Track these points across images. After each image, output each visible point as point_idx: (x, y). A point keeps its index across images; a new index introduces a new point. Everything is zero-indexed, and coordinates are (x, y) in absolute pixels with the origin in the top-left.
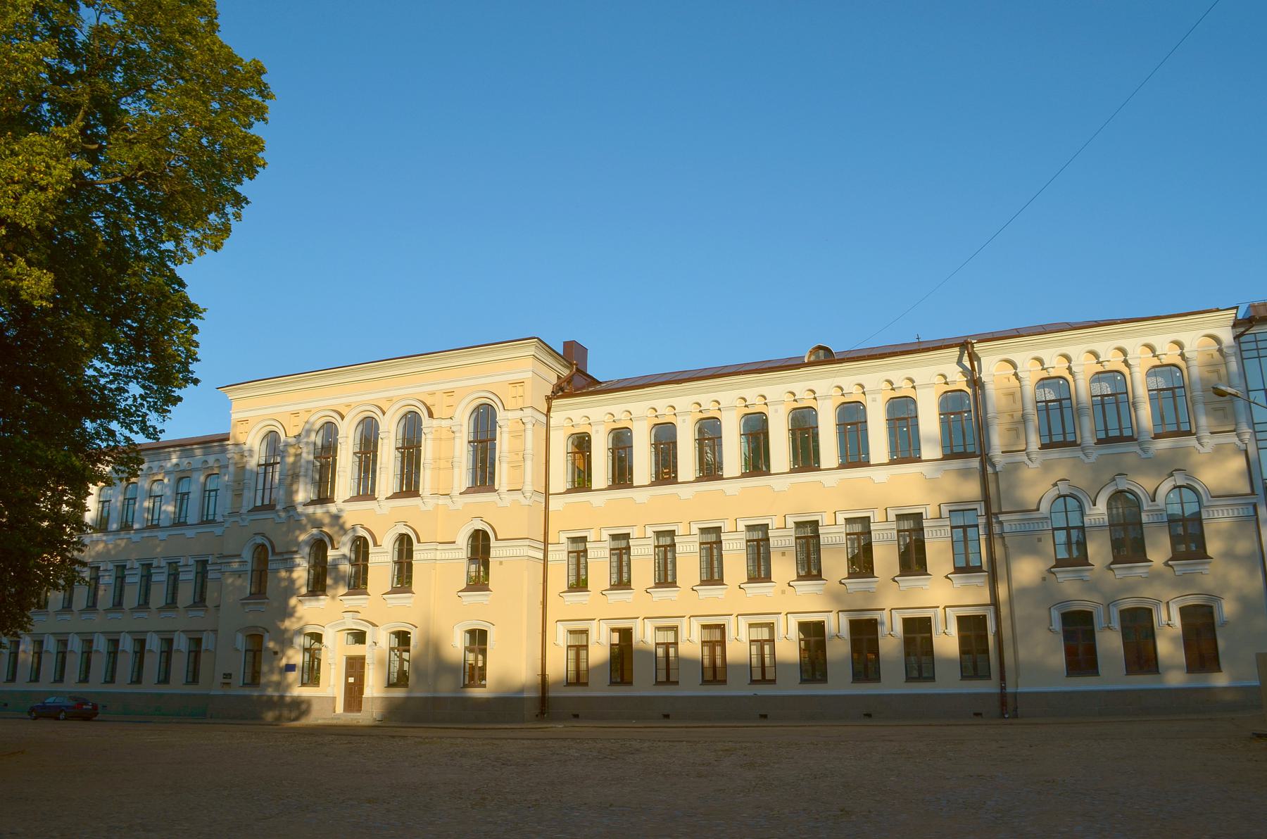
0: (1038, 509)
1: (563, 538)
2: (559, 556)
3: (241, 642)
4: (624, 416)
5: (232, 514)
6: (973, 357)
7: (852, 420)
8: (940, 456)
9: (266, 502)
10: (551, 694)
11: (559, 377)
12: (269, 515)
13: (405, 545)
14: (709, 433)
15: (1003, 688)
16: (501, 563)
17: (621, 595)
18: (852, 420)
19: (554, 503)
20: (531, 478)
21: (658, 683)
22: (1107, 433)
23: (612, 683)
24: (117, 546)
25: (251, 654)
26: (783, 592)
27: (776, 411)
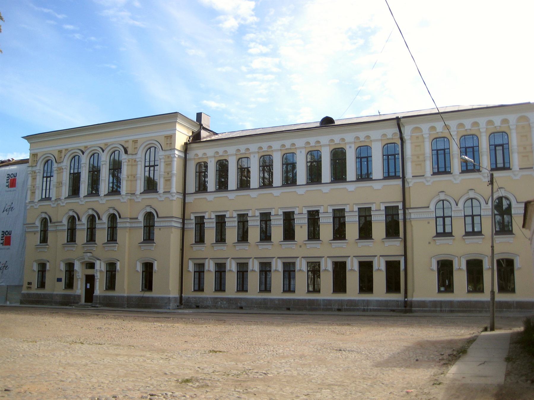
1: (193, 217)
2: (191, 225)
3: (35, 267)
5: (30, 202)
8: (381, 177)
9: (47, 196)
11: (193, 133)
12: (47, 203)
13: (113, 218)
19: (189, 199)
20: (176, 185)
21: (309, 291)
22: (395, 174)
23: (261, 291)
25: (197, 274)
26: (429, 243)
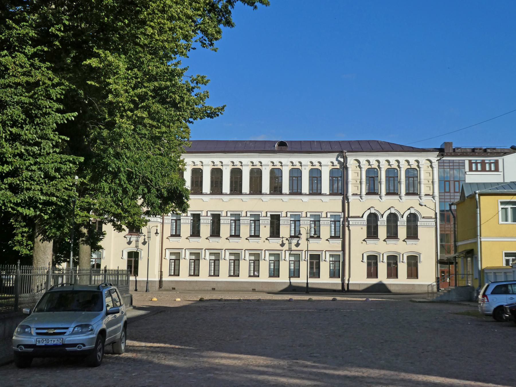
0: (362, 217)
4: (199, 163)
6: (345, 158)
7: (296, 175)
10: (309, 286)
14: (236, 174)
15: (161, 278)
16: (265, 227)
17: (194, 240)
18: (256, 175)
24: (17, 201)
26: (264, 242)
27: (265, 169)
